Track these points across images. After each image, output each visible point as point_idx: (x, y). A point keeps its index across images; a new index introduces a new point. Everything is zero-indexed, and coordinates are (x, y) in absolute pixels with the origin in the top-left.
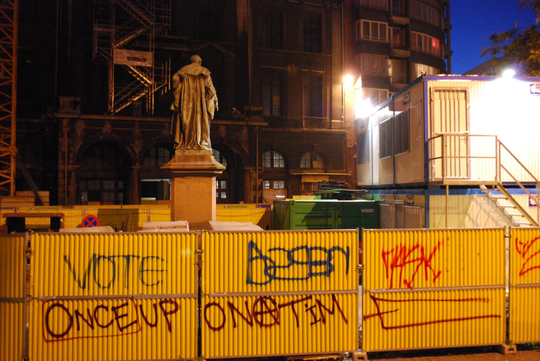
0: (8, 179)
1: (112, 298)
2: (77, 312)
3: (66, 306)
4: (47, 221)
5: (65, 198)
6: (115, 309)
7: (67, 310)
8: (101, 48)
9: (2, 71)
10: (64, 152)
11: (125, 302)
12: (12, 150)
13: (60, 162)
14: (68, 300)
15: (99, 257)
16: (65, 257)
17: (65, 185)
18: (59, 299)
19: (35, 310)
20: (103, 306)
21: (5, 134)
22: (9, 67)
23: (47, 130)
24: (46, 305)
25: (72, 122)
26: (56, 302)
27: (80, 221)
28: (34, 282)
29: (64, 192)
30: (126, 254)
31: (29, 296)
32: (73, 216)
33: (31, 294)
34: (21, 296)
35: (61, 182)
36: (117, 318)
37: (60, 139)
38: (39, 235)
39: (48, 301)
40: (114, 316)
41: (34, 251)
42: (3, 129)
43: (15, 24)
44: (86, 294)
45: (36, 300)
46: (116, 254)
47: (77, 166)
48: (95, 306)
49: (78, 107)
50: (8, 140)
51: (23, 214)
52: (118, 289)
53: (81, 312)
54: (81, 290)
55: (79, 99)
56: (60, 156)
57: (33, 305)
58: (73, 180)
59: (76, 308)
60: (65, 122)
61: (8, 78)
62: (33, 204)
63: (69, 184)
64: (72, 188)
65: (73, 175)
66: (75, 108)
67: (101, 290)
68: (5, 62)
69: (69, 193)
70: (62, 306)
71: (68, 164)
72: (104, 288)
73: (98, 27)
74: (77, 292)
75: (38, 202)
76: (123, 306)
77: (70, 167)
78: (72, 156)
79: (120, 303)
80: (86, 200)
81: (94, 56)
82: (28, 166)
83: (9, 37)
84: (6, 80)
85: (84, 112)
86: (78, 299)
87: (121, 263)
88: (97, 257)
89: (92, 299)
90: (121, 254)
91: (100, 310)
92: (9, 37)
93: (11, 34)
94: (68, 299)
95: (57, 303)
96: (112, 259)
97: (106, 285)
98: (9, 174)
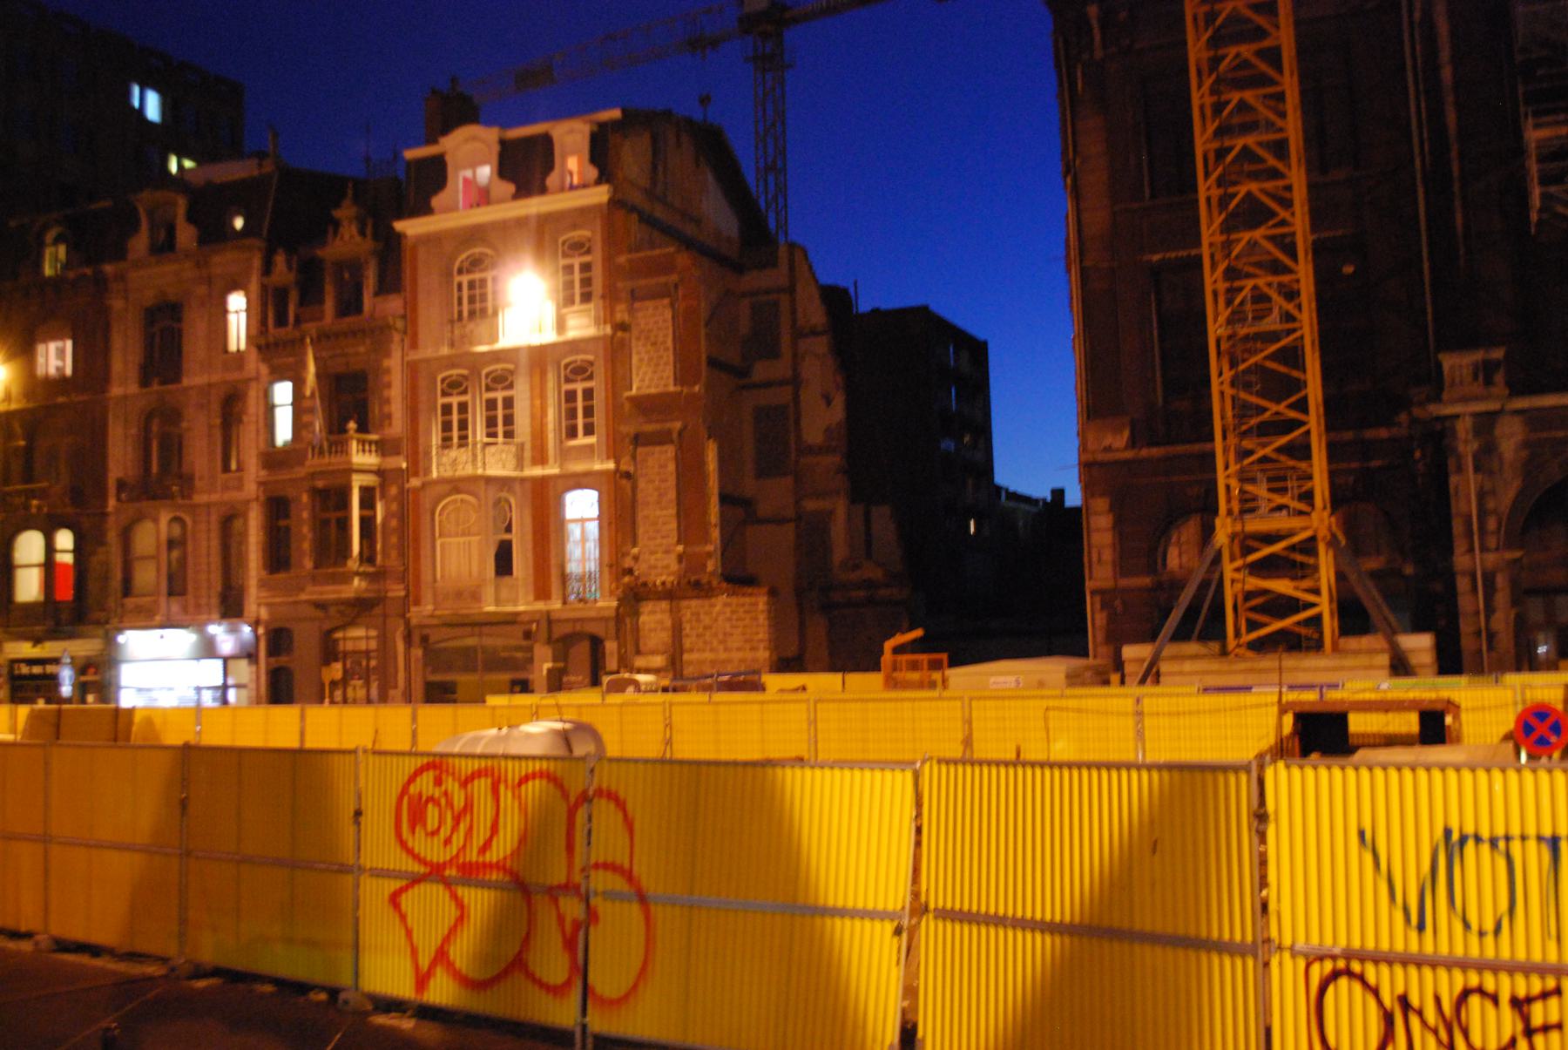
0: (1314, 605)
1: (1512, 968)
2: (1404, 1001)
3: (1371, 979)
4: (1409, 723)
5: (1480, 651)
6: (1520, 1005)
7: (1375, 992)
8: (1553, 189)
9: (1276, 312)
10: (1470, 516)
11: (1551, 983)
12: (1321, 521)
13: (1460, 546)
14: (1376, 962)
15: (1463, 839)
16: (1362, 834)
17: (1477, 613)
18: (1349, 955)
19: (1289, 984)
20: (1480, 990)
21: (1299, 479)
22: (1291, 294)
23: (1418, 454)
24: (1316, 970)
25: (1485, 423)
26: (1341, 964)
27: (1508, 722)
28: (1279, 900)
29: (1478, 633)
30: (1547, 832)
31: (1268, 941)
32: (1487, 706)
33: (1274, 933)
34: (1249, 938)
35: (1465, 603)
36: (1529, 1032)
37: (1454, 480)
38: (1288, 767)
39: (1321, 959)
40: (1520, 1026)
41: (1276, 812)
42: (1293, 468)
43: (1297, 178)
44: (1429, 948)
45: (1287, 955)
46: (1515, 831)
47: (1509, 555)
48: (1458, 988)
49: (1499, 377)
50: (1308, 497)
51: (1342, 702)
52: (1527, 941)
53: (1415, 1000)
54: (1414, 935)
55: (1498, 354)
56: (1458, 527)
57: (1280, 964)
58: (1502, 598)
59: (1400, 990)
60: (1464, 428)
61: (1290, 326)
62: (1386, 672)
63: (1490, 610)
64: (1502, 621)
65: (1501, 581)
66: (1488, 382)
67: (1474, 939)
68: (1280, 285)
69: (1491, 636)
70: (1361, 978)
71: (1484, 549)
72: (1481, 934)
73: (1537, 126)
74: (1403, 940)
75: (1400, 666)
76: (1544, 995)
77: (1491, 558)
78: (1492, 524)
79: (1537, 986)
80: (1553, 656)
81: (1534, 217)
82: (1372, 564)
83: (1283, 214)
84: (1290, 332)
85: (1516, 390)
86: (1406, 961)
87: (1533, 858)
88: (1455, 836)
89: (1450, 964)
90: (1531, 831)
91: (1475, 1000)
92: (1283, 214)
93: (1287, 204)
94: (1377, 959)
95: (1345, 967)
96: (1502, 844)
97: (1489, 925)
98: (1316, 591)
